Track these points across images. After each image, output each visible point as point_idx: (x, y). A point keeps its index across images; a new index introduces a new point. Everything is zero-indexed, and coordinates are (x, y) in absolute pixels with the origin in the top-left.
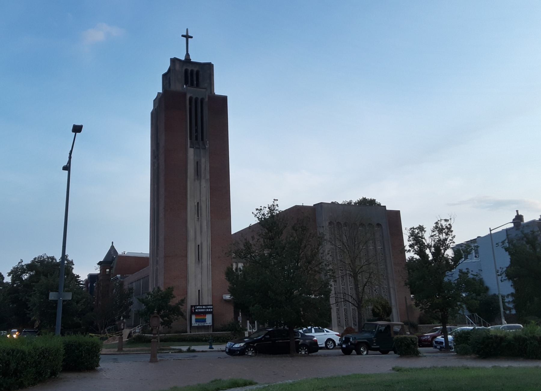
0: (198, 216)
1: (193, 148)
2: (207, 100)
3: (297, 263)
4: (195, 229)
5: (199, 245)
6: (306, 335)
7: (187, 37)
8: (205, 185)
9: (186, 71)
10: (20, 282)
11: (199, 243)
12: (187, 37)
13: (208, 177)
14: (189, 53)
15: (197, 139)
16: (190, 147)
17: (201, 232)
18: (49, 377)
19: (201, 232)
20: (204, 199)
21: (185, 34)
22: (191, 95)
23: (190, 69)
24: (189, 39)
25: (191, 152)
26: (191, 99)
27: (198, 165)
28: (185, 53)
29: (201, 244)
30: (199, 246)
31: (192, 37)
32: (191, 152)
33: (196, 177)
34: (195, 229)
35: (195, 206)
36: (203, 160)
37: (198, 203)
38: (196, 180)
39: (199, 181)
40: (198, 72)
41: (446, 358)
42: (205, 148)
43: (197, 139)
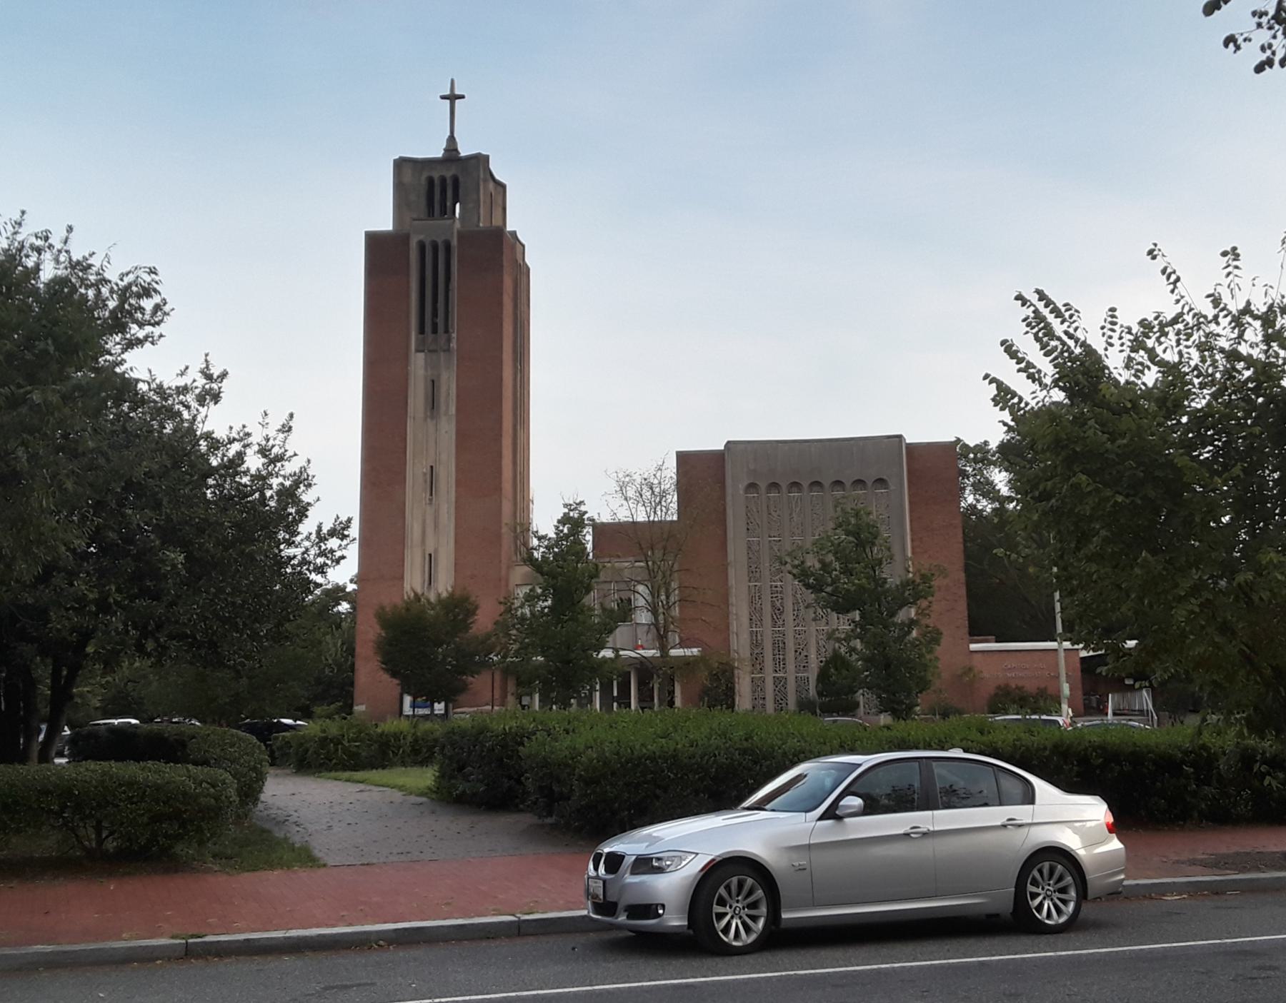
0: (431, 494)
1: (423, 351)
2: (455, 242)
3: (662, 633)
4: (424, 522)
5: (430, 555)
6: (282, 723)
7: (453, 98)
8: (447, 429)
9: (431, 181)
10: (1185, 629)
11: (430, 549)
12: (453, 98)
13: (453, 410)
14: (455, 136)
15: (435, 331)
16: (417, 351)
17: (436, 526)
18: (1007, 992)
19: (436, 526)
20: (444, 457)
21: (448, 92)
22: (421, 237)
23: (436, 175)
24: (457, 101)
25: (418, 361)
26: (422, 246)
27: (433, 385)
28: (448, 134)
29: (436, 551)
30: (430, 555)
31: (462, 97)
32: (418, 361)
33: (429, 414)
34: (424, 522)
35: (425, 474)
36: (444, 376)
37: (432, 467)
38: (429, 420)
39: (435, 422)
40: (456, 181)
41: (370, 790)
42: (448, 350)
43: (435, 331)
